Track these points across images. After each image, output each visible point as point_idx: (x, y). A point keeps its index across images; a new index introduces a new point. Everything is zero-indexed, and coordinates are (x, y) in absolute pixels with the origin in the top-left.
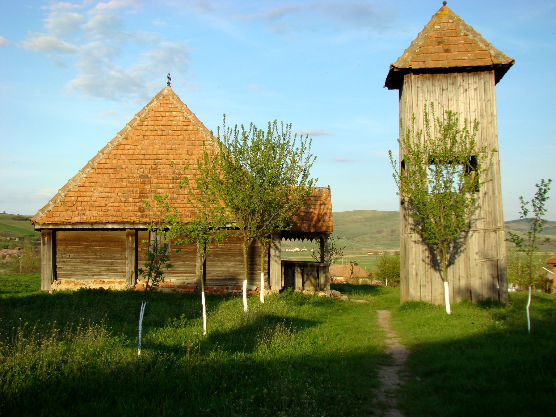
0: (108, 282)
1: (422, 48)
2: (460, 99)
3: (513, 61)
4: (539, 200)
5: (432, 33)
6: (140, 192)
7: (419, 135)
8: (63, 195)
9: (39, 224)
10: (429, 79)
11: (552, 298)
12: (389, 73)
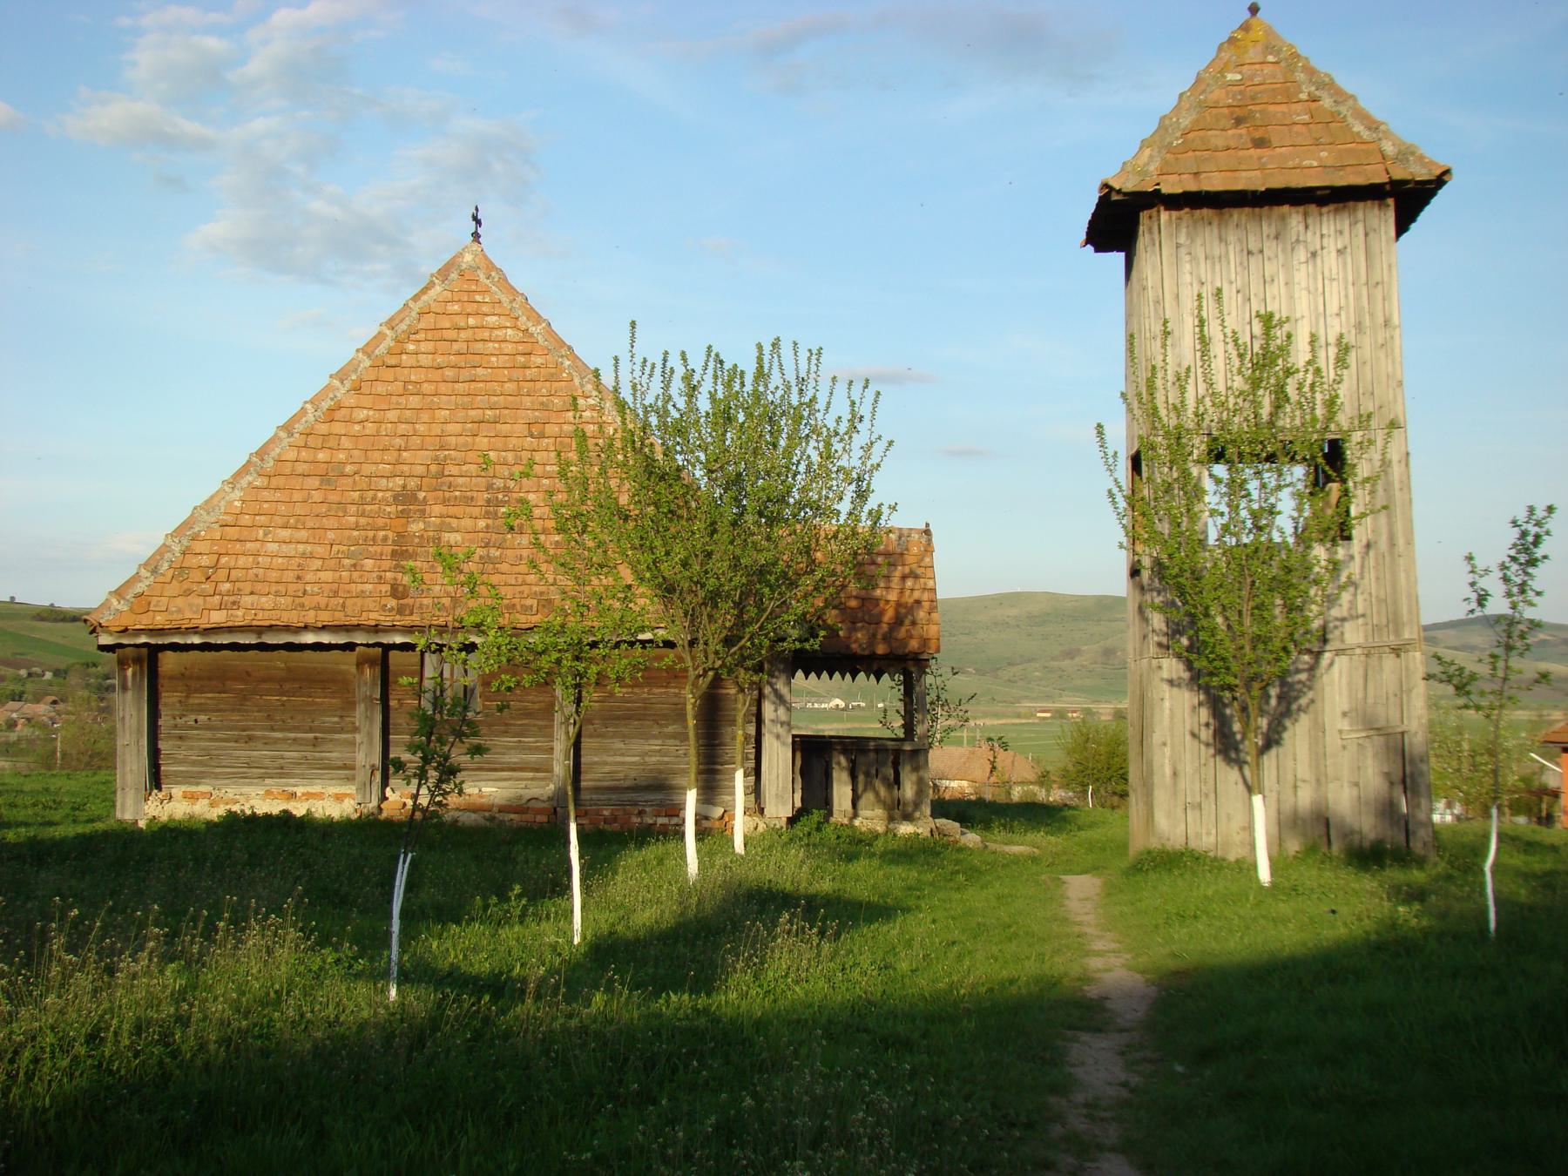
0: (303, 794)
1: (1191, 136)
2: (1296, 280)
3: (1447, 172)
4: (1521, 564)
5: (1217, 94)
6: (394, 541)
7: (1181, 381)
8: (177, 549)
9: (110, 633)
10: (1210, 223)
11: (1556, 841)
12: (1098, 205)
